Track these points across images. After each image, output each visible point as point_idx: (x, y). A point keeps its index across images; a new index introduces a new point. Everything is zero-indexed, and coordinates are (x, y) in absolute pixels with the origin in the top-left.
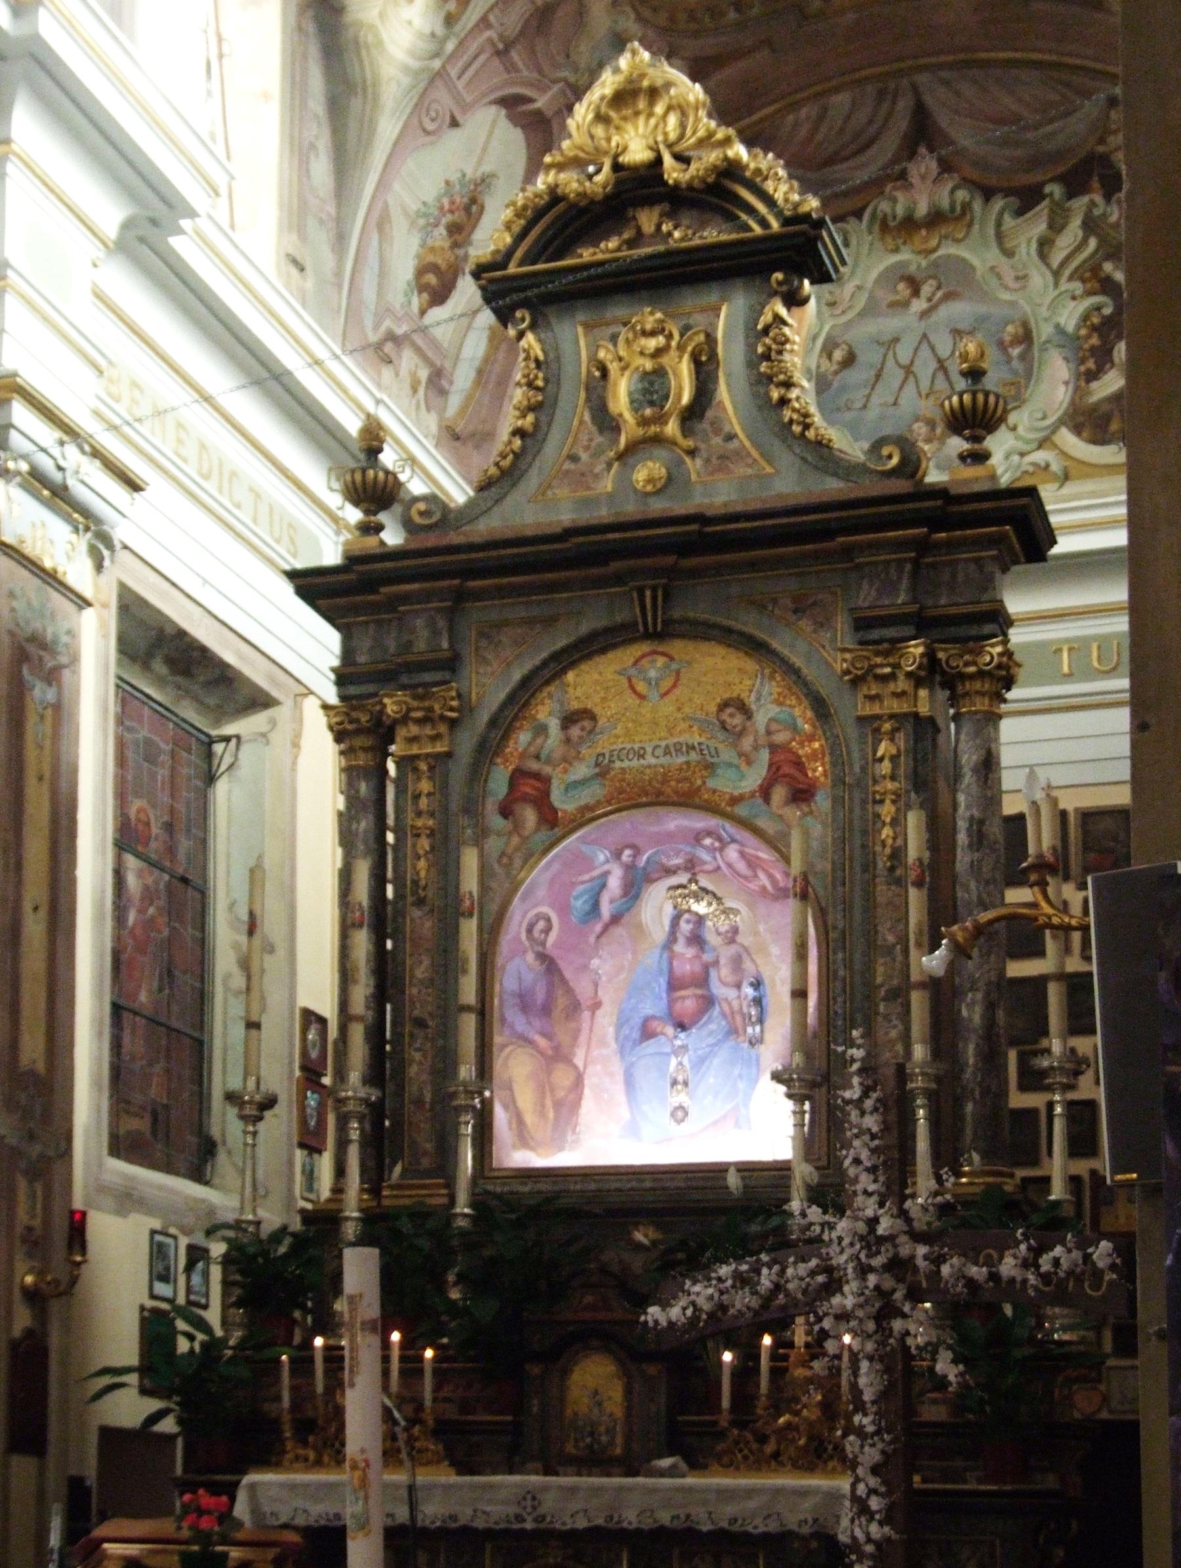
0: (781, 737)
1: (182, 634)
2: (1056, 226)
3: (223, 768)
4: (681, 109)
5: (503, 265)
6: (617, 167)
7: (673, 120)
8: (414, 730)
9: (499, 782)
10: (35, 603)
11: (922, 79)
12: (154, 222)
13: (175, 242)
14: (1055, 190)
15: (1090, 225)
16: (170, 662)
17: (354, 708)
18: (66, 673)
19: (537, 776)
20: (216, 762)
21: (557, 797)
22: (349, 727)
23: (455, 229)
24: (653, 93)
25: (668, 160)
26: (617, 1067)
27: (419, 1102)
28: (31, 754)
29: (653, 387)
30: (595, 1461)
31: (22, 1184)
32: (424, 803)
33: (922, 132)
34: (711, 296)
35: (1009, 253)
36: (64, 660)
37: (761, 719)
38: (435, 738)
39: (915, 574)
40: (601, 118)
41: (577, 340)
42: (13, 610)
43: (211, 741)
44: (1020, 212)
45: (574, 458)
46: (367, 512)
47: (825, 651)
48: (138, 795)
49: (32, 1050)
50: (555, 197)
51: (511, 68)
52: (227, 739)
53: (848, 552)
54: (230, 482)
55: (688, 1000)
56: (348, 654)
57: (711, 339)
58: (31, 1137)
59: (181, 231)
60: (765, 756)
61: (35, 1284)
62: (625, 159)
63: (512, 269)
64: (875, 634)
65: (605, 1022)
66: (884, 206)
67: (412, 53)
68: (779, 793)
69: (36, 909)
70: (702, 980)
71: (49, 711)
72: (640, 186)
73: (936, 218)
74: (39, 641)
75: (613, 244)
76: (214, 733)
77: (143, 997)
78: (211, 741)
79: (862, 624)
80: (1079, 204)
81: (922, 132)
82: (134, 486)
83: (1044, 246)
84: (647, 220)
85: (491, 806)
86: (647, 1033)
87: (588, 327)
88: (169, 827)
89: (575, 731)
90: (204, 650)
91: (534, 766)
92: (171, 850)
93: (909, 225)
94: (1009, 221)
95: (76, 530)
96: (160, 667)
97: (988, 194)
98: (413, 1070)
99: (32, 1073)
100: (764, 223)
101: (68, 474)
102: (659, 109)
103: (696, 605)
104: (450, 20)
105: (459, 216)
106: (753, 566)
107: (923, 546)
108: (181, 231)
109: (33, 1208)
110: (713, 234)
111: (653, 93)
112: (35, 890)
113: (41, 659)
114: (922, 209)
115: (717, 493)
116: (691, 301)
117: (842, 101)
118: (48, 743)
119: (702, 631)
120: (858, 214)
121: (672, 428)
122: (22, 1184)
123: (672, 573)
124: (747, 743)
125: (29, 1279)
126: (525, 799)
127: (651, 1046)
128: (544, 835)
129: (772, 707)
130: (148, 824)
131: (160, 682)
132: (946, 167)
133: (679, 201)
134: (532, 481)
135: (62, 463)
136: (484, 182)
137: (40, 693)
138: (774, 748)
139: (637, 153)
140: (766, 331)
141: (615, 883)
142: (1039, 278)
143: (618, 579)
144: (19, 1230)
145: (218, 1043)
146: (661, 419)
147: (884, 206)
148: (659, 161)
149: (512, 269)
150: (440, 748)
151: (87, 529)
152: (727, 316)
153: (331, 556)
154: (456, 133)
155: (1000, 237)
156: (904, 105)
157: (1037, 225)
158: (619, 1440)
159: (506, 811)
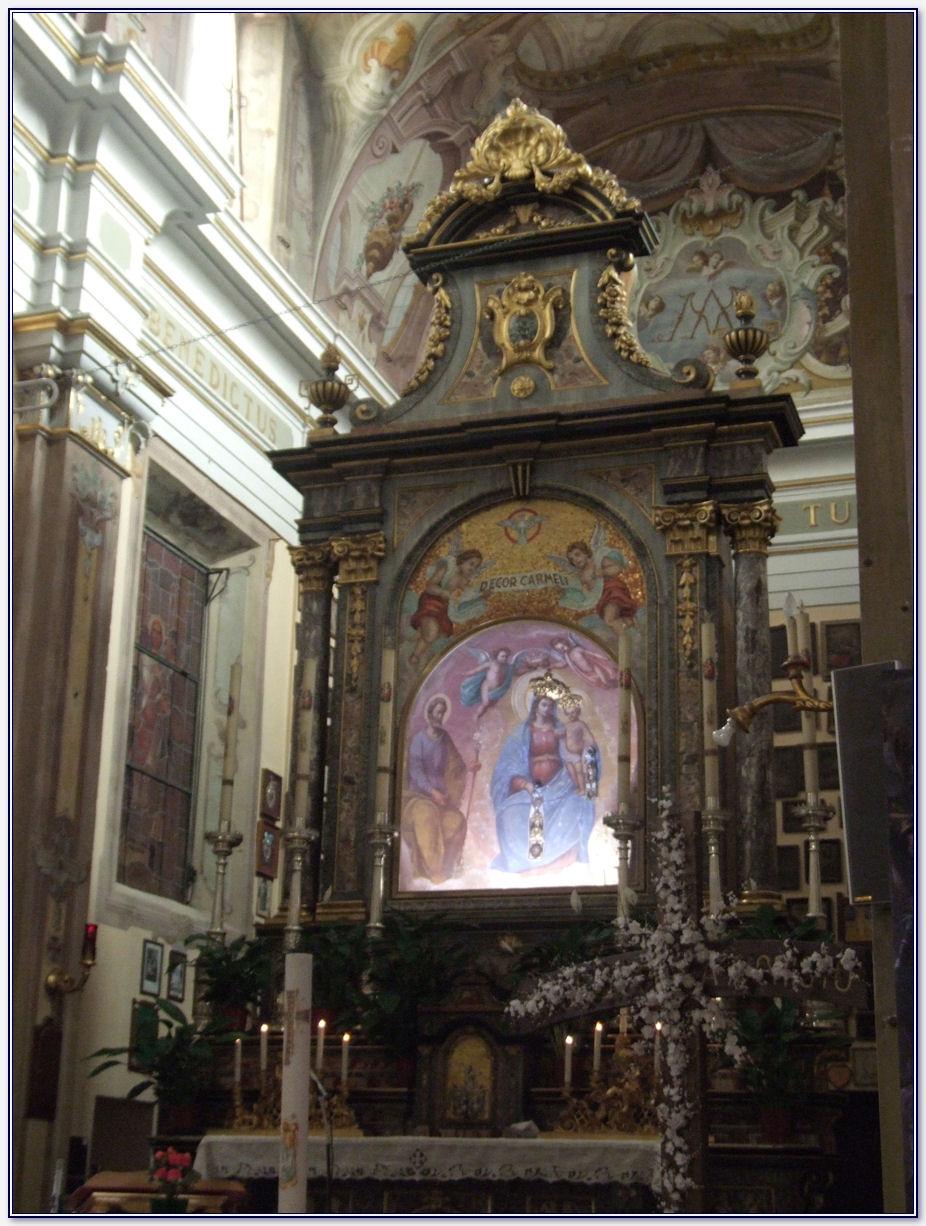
0: (612, 570)
1: (192, 496)
2: (801, 218)
3: (216, 591)
4: (547, 141)
5: (425, 244)
6: (503, 179)
7: (541, 149)
8: (353, 564)
9: (411, 603)
10: (91, 475)
11: (709, 122)
12: (189, 215)
13: (204, 229)
14: (800, 195)
15: (823, 218)
16: (183, 516)
17: (311, 549)
18: (109, 524)
19: (438, 598)
20: (211, 588)
21: (453, 614)
22: (306, 562)
23: (392, 220)
24: (529, 131)
25: (538, 175)
26: (492, 815)
27: (346, 841)
28: (80, 581)
29: (525, 327)
30: (469, 1125)
31: (52, 904)
32: (357, 617)
33: (710, 157)
34: (566, 263)
35: (769, 237)
36: (108, 514)
37: (598, 557)
38: (367, 571)
39: (706, 455)
40: (493, 147)
41: (474, 294)
42: (75, 479)
43: (209, 573)
44: (776, 209)
45: (470, 374)
46: (325, 411)
47: (644, 509)
48: (154, 612)
49: (66, 801)
50: (461, 199)
51: (434, 115)
52: (220, 571)
53: (659, 439)
54: (232, 390)
55: (544, 765)
56: (308, 510)
57: (565, 293)
58: (61, 867)
59: (207, 221)
60: (600, 583)
61: (56, 982)
62: (509, 174)
63: (431, 246)
64: (678, 497)
65: (484, 779)
66: (684, 205)
67: (367, 105)
68: (611, 611)
69: (76, 695)
70: (554, 749)
71: (95, 552)
72: (519, 192)
73: (719, 213)
74: (91, 501)
75: (500, 230)
76: (211, 567)
77: (149, 761)
78: (209, 573)
79: (669, 490)
80: (816, 204)
81: (710, 157)
82: (164, 392)
83: (793, 231)
84: (523, 214)
85: (405, 620)
86: (514, 788)
87: (482, 285)
88: (175, 635)
89: (466, 566)
90: (207, 508)
91: (437, 591)
92: (175, 652)
93: (701, 217)
94: (768, 215)
95: (122, 424)
96: (175, 519)
97: (754, 197)
98: (342, 817)
99: (65, 819)
100: (603, 216)
101: (120, 384)
102: (533, 142)
103: (553, 476)
104: (394, 84)
105: (396, 211)
106: (593, 449)
107: (712, 436)
108: (207, 221)
109: (59, 922)
110: (568, 223)
111: (529, 131)
112: (76, 681)
113: (92, 514)
114: (710, 207)
115: (568, 398)
116: (553, 267)
117: (655, 136)
118: (93, 574)
119: (558, 495)
120: (666, 210)
121: (538, 353)
122: (52, 904)
123: (537, 454)
124: (588, 574)
125: (52, 978)
126: (429, 614)
127: (516, 799)
128: (442, 641)
129: (606, 548)
130: (160, 633)
131: (175, 531)
132: (726, 180)
133: (545, 201)
134: (440, 390)
135: (115, 377)
136: (414, 189)
137: (90, 538)
138: (607, 578)
139: (517, 170)
140: (603, 288)
141: (492, 676)
142: (789, 253)
143: (499, 458)
144: (47, 939)
145: (201, 796)
146: (531, 348)
147: (684, 205)
148: (532, 175)
149: (431, 246)
150: (371, 578)
151: (130, 423)
152: (576, 278)
153: (299, 442)
154: (396, 158)
155: (762, 226)
156: (697, 139)
157: (788, 217)
158: (487, 1108)
159: (416, 624)
